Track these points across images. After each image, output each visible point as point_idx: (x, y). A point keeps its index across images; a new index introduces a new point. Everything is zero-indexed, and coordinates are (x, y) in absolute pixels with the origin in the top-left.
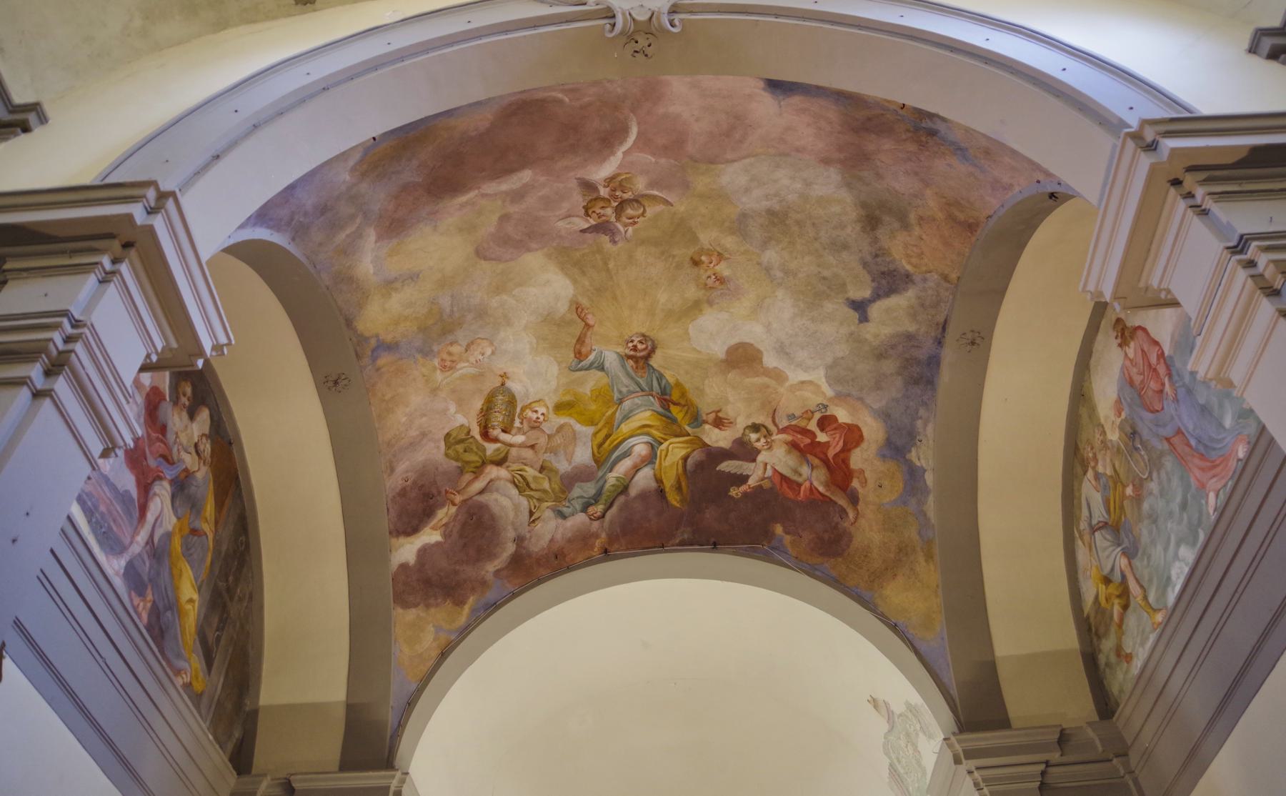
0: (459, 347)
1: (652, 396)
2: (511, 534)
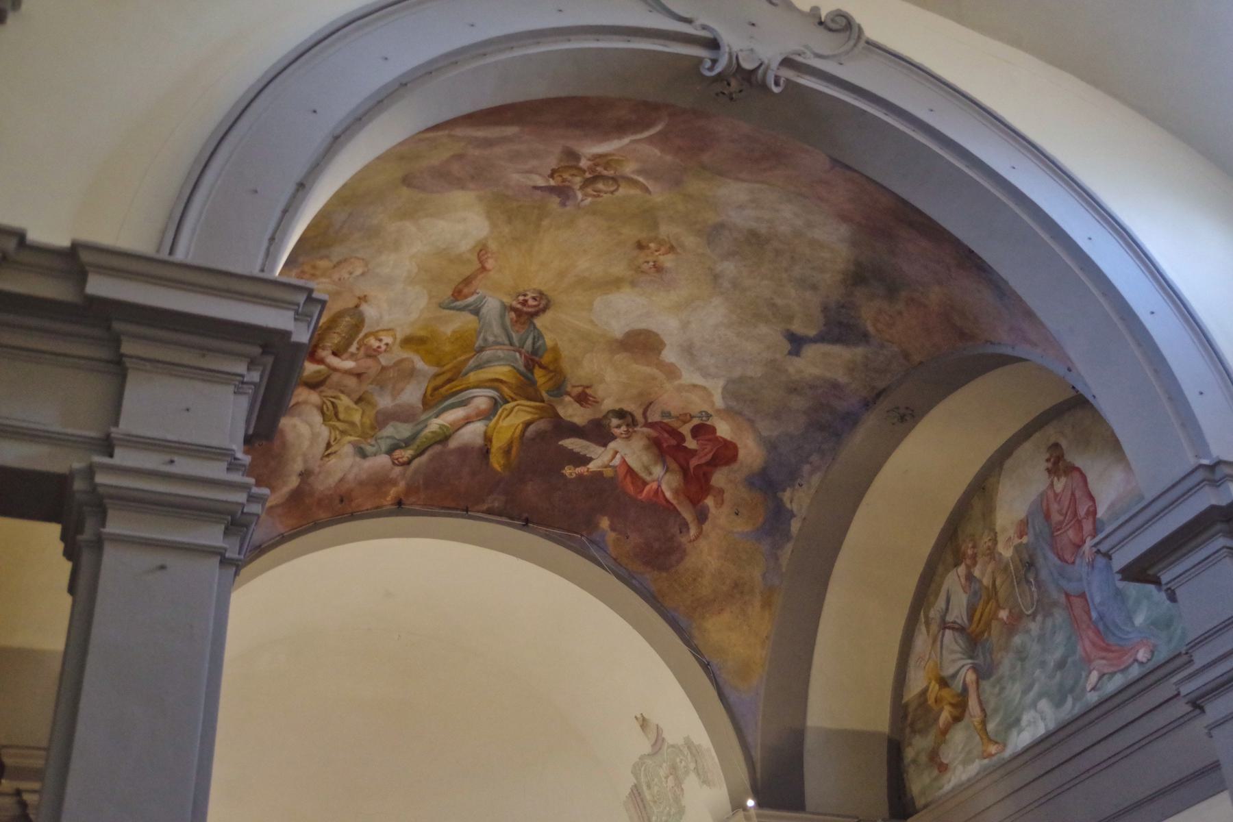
1: (520, 353)
2: (298, 466)
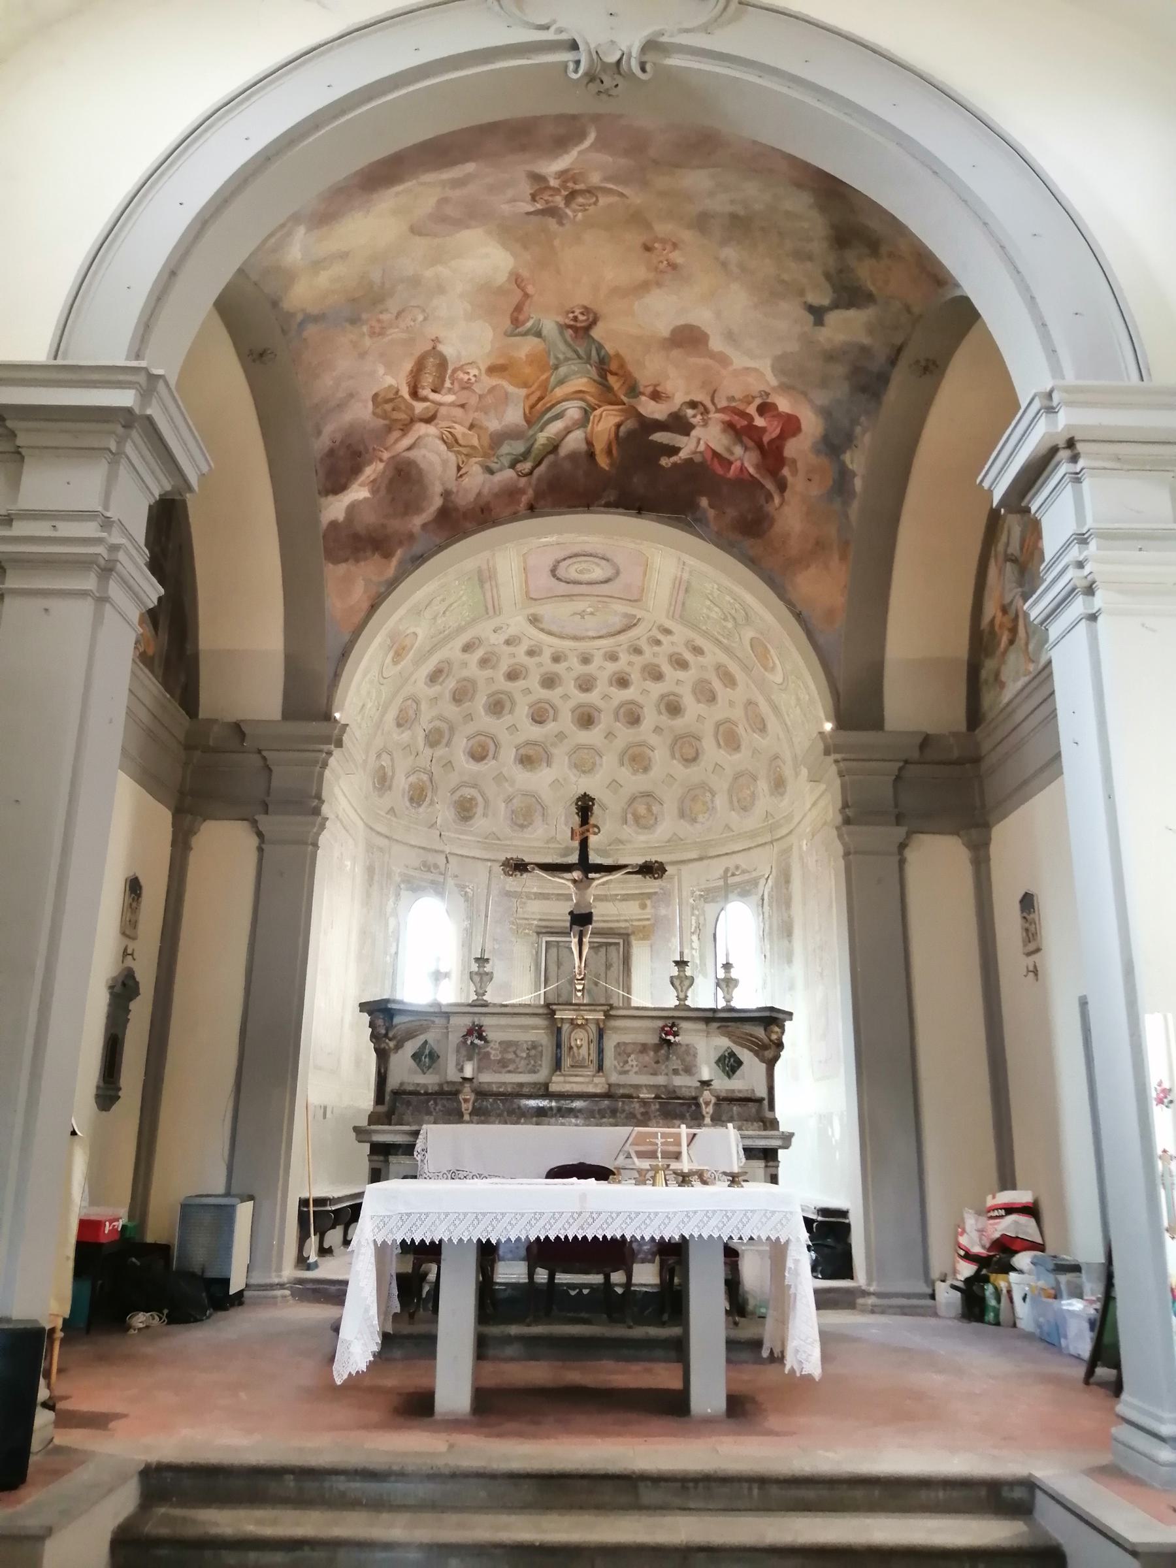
0: (389, 315)
2: (438, 489)
